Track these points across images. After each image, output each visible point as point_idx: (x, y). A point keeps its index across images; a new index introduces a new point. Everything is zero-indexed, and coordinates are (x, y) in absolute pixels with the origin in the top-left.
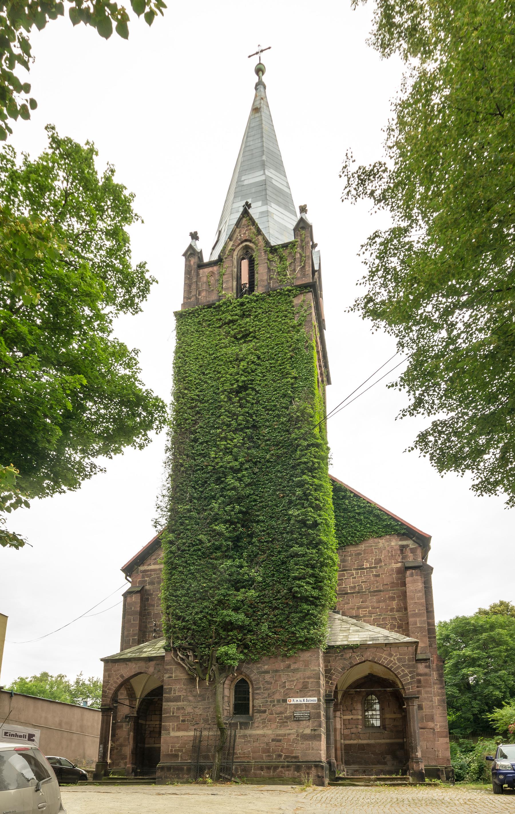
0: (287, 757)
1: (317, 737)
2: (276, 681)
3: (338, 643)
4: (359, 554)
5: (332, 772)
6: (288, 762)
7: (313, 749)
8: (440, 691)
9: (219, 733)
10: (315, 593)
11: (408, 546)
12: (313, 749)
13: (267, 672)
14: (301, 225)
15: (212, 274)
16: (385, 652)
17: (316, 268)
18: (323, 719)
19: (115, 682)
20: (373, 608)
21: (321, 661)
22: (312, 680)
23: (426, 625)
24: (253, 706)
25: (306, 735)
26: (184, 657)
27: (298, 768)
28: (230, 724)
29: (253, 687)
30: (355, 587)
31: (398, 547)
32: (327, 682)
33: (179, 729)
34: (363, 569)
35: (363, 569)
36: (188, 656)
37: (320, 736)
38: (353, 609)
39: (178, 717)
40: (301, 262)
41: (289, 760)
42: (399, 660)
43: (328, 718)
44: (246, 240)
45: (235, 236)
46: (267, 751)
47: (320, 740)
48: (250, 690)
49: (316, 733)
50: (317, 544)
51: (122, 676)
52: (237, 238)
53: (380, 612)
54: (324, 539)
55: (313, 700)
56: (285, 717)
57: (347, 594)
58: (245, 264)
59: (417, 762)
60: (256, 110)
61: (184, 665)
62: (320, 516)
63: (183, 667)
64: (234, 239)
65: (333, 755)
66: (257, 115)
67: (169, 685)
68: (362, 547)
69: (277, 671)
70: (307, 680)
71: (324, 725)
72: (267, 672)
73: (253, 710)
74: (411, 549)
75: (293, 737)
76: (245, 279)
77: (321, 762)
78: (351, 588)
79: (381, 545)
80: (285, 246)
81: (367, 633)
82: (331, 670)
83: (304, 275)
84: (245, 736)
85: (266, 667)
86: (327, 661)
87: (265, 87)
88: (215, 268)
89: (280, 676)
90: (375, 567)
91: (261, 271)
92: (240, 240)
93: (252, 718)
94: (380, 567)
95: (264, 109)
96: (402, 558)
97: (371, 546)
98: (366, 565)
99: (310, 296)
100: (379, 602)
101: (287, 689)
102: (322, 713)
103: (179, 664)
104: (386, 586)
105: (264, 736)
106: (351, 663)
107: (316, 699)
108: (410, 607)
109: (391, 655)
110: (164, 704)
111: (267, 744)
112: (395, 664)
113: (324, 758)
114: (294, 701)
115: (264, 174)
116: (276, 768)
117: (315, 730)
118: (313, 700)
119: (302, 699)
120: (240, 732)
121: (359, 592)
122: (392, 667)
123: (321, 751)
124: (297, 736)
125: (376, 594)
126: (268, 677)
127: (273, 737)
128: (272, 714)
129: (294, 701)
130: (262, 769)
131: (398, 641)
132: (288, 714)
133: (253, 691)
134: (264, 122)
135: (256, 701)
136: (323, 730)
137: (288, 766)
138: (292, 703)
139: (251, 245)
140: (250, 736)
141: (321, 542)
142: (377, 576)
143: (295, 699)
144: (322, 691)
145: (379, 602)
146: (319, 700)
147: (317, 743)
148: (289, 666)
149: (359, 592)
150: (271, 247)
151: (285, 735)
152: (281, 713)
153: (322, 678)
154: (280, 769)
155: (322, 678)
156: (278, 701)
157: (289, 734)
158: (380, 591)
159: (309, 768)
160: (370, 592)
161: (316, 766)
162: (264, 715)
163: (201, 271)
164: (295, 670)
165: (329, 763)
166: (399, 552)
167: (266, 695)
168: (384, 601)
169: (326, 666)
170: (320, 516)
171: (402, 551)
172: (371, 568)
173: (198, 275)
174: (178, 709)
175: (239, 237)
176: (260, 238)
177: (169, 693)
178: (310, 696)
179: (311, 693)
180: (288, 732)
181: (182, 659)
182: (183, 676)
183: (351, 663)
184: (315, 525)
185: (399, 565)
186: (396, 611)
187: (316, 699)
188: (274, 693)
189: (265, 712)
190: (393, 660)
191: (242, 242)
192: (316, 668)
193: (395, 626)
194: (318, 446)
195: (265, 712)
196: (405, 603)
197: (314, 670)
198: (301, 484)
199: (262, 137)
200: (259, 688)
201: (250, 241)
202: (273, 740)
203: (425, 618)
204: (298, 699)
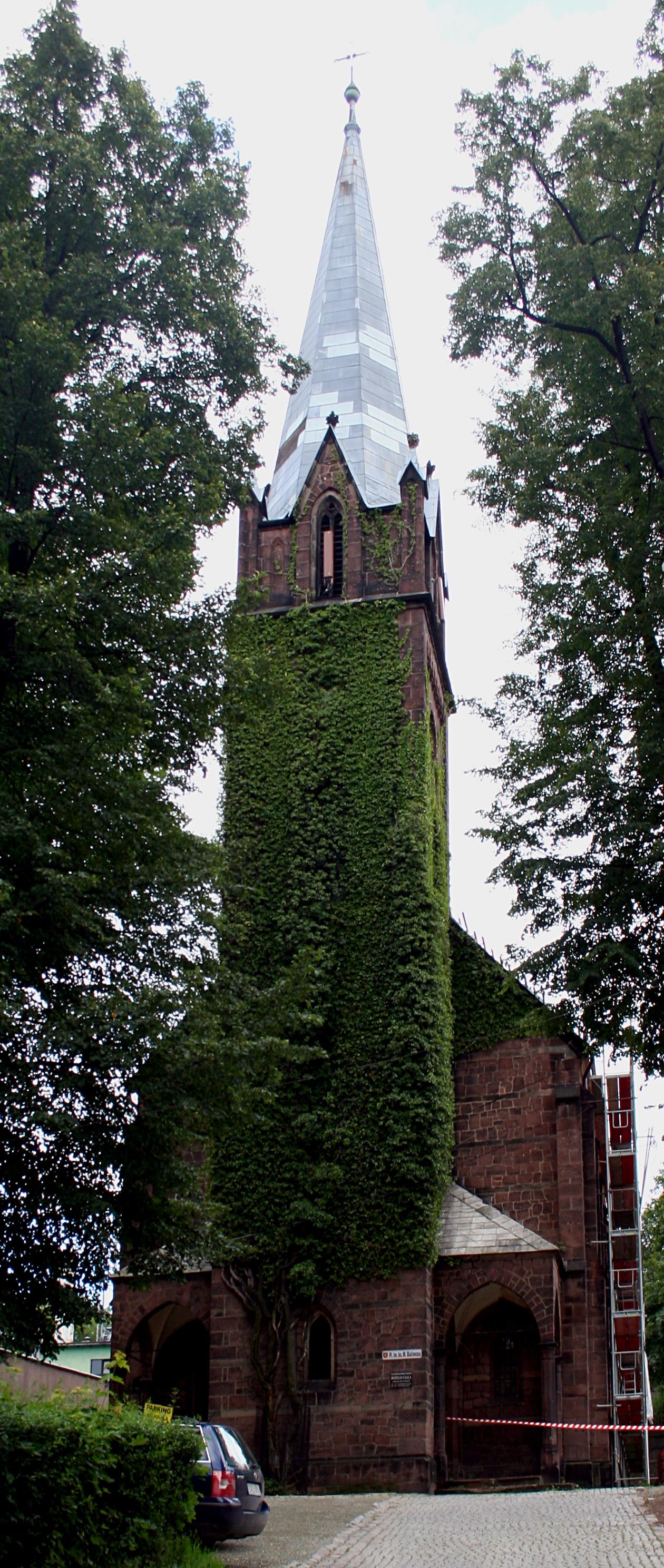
0: (380, 1449)
1: (419, 1415)
2: (368, 1321)
3: (454, 1252)
4: (492, 1068)
5: (441, 1474)
6: (382, 1457)
7: (415, 1435)
8: (598, 1327)
9: (291, 1411)
10: (421, 1172)
11: (561, 1055)
12: (415, 1435)
13: (355, 1306)
14: (410, 475)
15: (278, 542)
16: (515, 1268)
17: (432, 534)
18: (429, 1384)
19: (132, 1320)
20: (510, 1173)
21: (428, 1285)
22: (416, 1320)
23: (582, 1208)
24: (336, 1364)
25: (406, 1412)
26: (240, 1280)
27: (395, 1468)
28: (305, 1396)
29: (335, 1332)
30: (485, 1131)
31: (547, 1058)
32: (437, 1320)
33: (233, 1406)
34: (499, 1097)
35: (499, 1097)
36: (245, 1278)
37: (424, 1412)
38: (482, 1174)
39: (232, 1385)
40: (410, 546)
41: (383, 1453)
42: (533, 1281)
43: (436, 1382)
44: (331, 489)
45: (315, 478)
46: (354, 1440)
47: (424, 1421)
48: (332, 1337)
49: (420, 1408)
50: (425, 1088)
51: (141, 1309)
52: (317, 482)
53: (520, 1181)
54: (432, 1078)
55: (416, 1353)
56: (380, 1383)
57: (473, 1144)
58: (328, 536)
59: (550, 1453)
60: (346, 187)
61: (240, 1294)
62: (429, 1037)
63: (236, 1295)
64: (313, 484)
65: (443, 1449)
66: (347, 200)
67: (218, 1328)
68: (497, 1054)
69: (368, 1304)
70: (408, 1320)
71: (431, 1395)
72: (355, 1306)
73: (336, 1371)
74: (566, 1062)
75: (389, 1416)
76: (328, 571)
77: (425, 1455)
78: (482, 1134)
79: (523, 1052)
80: (387, 510)
81: (493, 1231)
82: (442, 1298)
83: (414, 571)
84: (324, 1416)
85: (354, 1297)
86: (436, 1283)
87: (358, 131)
88: (284, 533)
89: (373, 1312)
90: (514, 1095)
91: (351, 552)
92: (321, 486)
93: (333, 1386)
94: (522, 1095)
95: (358, 190)
96: (554, 1080)
97: (509, 1054)
98: (502, 1090)
99: (422, 615)
100: (518, 1161)
101: (384, 1335)
102: (429, 1374)
103: (232, 1291)
104: (529, 1133)
105: (350, 1415)
106: (469, 1287)
107: (420, 1351)
108: (562, 1173)
109: (522, 1273)
110: (212, 1361)
111: (355, 1429)
112: (527, 1288)
113: (429, 1450)
114: (392, 1355)
115: (358, 340)
116: (366, 1467)
117: (418, 1404)
118: (416, 1353)
119: (401, 1352)
120: (315, 1409)
121: (490, 1143)
122: (523, 1293)
123: (425, 1436)
124: (395, 1414)
125: (515, 1145)
126: (356, 1314)
127: (362, 1416)
128: (361, 1378)
129: (392, 1355)
130: (347, 1470)
131: (532, 1249)
132: (383, 1377)
133: (336, 1337)
134: (358, 219)
135: (340, 1357)
136: (429, 1402)
137: (382, 1464)
138: (388, 1358)
139: (337, 497)
140: (332, 1415)
141: (427, 1086)
142: (517, 1112)
143: (393, 1352)
144: (428, 1338)
145: (518, 1161)
146: (424, 1353)
147: (421, 1425)
148: (385, 1296)
149: (490, 1143)
150: (367, 510)
151: (378, 1413)
152: (374, 1376)
153: (429, 1314)
154: (371, 1469)
155: (429, 1314)
156: (370, 1356)
157: (384, 1411)
158: (520, 1141)
159: (409, 1466)
160: (506, 1143)
161: (419, 1463)
162: (351, 1380)
163: (264, 535)
164: (395, 1302)
165: (437, 1457)
166: (549, 1067)
167: (354, 1346)
168: (526, 1160)
169: (436, 1292)
170: (429, 1037)
171: (553, 1064)
172: (508, 1096)
173: (259, 541)
174: (232, 1370)
175: (321, 482)
176: (350, 487)
177: (219, 1343)
178: (413, 1348)
179: (413, 1342)
180: (382, 1407)
181: (237, 1283)
182: (238, 1313)
183: (469, 1287)
184: (422, 1053)
185: (549, 1092)
186: (544, 1180)
187: (420, 1351)
188: (365, 1342)
189: (352, 1374)
190: (522, 1282)
191: (324, 492)
192: (422, 1300)
193: (540, 1207)
194: (427, 907)
195: (351, 1374)
196: (555, 1166)
197: (419, 1303)
198: (406, 978)
199: (355, 254)
200: (344, 1335)
201: (338, 492)
202: (362, 1422)
203: (582, 1195)
204: (397, 1352)
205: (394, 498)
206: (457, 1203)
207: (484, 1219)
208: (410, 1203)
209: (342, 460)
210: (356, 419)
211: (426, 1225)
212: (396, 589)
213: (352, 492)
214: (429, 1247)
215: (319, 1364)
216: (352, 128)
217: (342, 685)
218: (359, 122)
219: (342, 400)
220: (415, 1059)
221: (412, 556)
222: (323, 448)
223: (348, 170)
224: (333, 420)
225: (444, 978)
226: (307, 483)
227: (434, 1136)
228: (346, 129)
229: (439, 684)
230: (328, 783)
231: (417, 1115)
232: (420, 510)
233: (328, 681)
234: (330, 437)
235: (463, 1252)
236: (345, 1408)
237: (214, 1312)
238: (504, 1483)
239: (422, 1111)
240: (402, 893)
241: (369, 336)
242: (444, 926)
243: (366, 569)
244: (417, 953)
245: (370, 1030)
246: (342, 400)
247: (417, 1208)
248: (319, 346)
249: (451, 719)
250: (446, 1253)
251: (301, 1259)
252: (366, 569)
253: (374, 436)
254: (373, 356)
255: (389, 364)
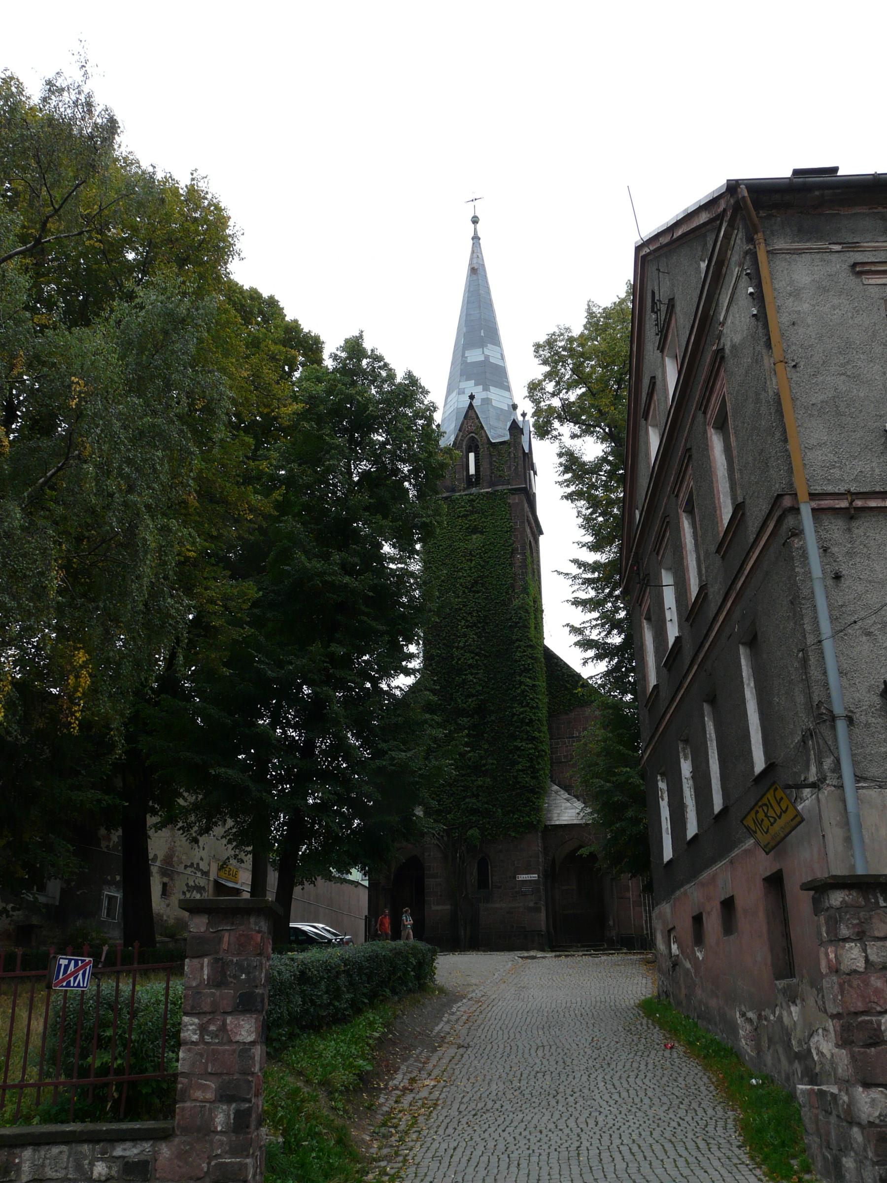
1: (537, 910)
17: (527, 451)
55: (534, 877)
57: (561, 762)
62: (534, 713)
66: (475, 277)
68: (572, 715)
91: (485, 465)
95: (480, 271)
113: (544, 928)
114: (522, 877)
118: (534, 877)
129: (522, 877)
170: (534, 713)
195: (499, 887)
199: (480, 306)
205: (507, 438)
206: (553, 794)
207: (569, 804)
208: (531, 798)
209: (478, 418)
210: (484, 395)
211: (538, 809)
212: (509, 484)
213: (483, 434)
214: (539, 821)
215: (483, 883)
216: (476, 238)
217: (482, 533)
218: (479, 235)
219: (476, 385)
220: (527, 724)
221: (516, 467)
222: (467, 412)
223: (475, 261)
224: (472, 397)
225: (542, 684)
226: (460, 430)
227: (539, 764)
228: (473, 239)
229: (534, 525)
230: (476, 582)
231: (530, 754)
232: (520, 444)
233: (475, 530)
234: (471, 406)
235: (557, 823)
236: (497, 905)
237: (426, 854)
238: (584, 946)
239: (532, 751)
240: (517, 640)
241: (490, 351)
242: (540, 656)
243: (492, 473)
244: (527, 670)
245: (195, 431)
246: (476, 385)
247: (532, 801)
248: (463, 356)
249: (541, 538)
250: (548, 823)
251: (471, 828)
252: (492, 473)
253: (494, 403)
254: (492, 360)
255: (500, 363)
